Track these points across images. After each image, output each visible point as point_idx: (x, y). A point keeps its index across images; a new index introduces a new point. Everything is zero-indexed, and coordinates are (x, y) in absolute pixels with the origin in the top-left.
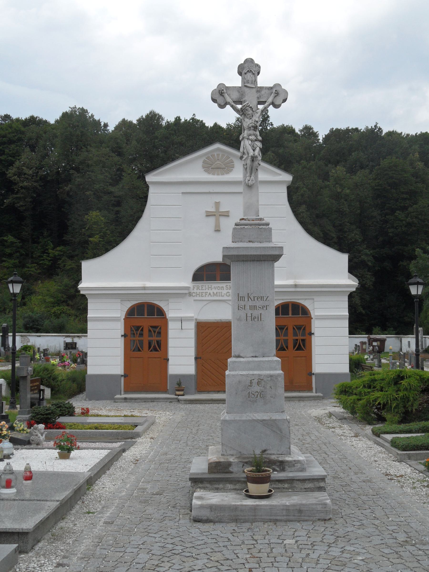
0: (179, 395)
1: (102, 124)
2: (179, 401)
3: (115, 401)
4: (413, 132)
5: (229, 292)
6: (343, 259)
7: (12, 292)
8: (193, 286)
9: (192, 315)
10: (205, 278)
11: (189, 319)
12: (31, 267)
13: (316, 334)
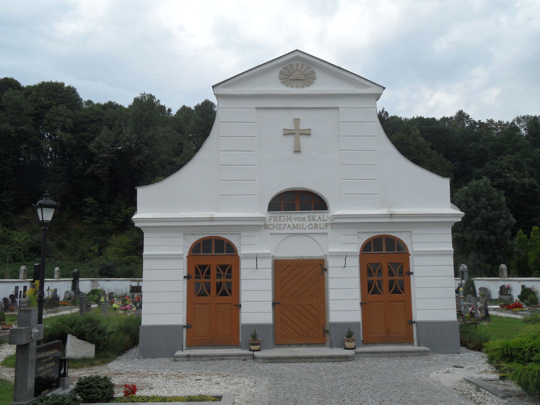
0: (254, 351)
1: (167, 109)
2: (254, 357)
3: (176, 359)
4: (410, 117)
5: (311, 224)
6: (445, 184)
7: (41, 219)
8: (270, 217)
9: (269, 251)
10: (282, 208)
11: (265, 256)
12: (108, 224)
13: (416, 274)
